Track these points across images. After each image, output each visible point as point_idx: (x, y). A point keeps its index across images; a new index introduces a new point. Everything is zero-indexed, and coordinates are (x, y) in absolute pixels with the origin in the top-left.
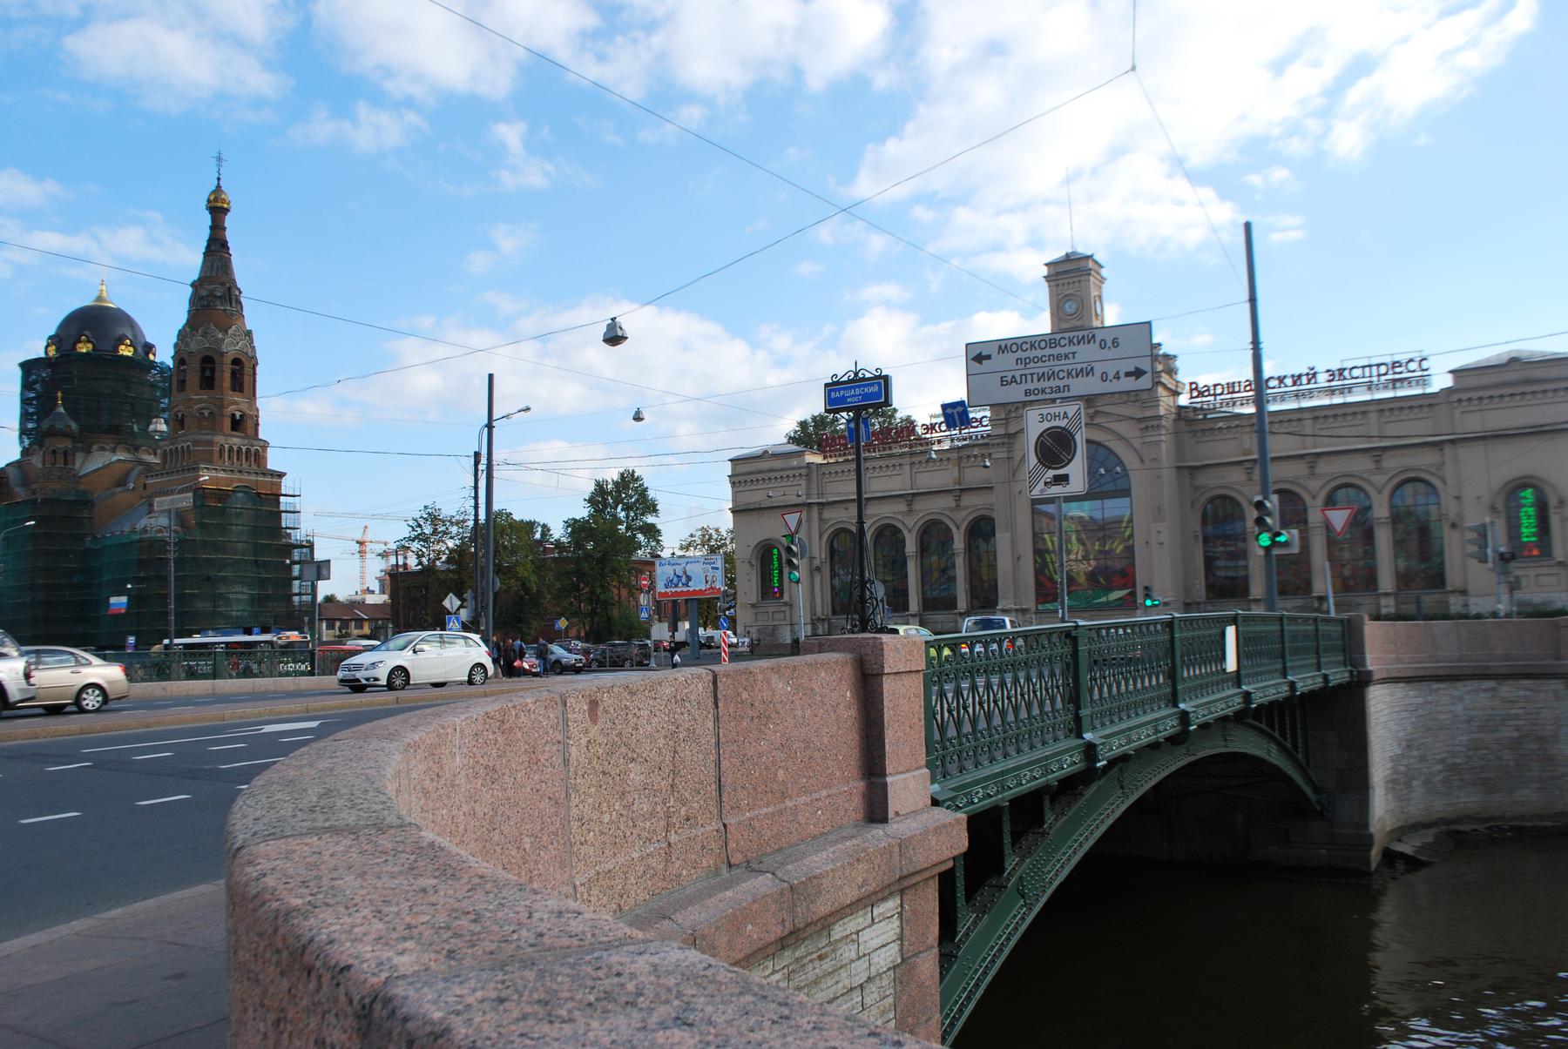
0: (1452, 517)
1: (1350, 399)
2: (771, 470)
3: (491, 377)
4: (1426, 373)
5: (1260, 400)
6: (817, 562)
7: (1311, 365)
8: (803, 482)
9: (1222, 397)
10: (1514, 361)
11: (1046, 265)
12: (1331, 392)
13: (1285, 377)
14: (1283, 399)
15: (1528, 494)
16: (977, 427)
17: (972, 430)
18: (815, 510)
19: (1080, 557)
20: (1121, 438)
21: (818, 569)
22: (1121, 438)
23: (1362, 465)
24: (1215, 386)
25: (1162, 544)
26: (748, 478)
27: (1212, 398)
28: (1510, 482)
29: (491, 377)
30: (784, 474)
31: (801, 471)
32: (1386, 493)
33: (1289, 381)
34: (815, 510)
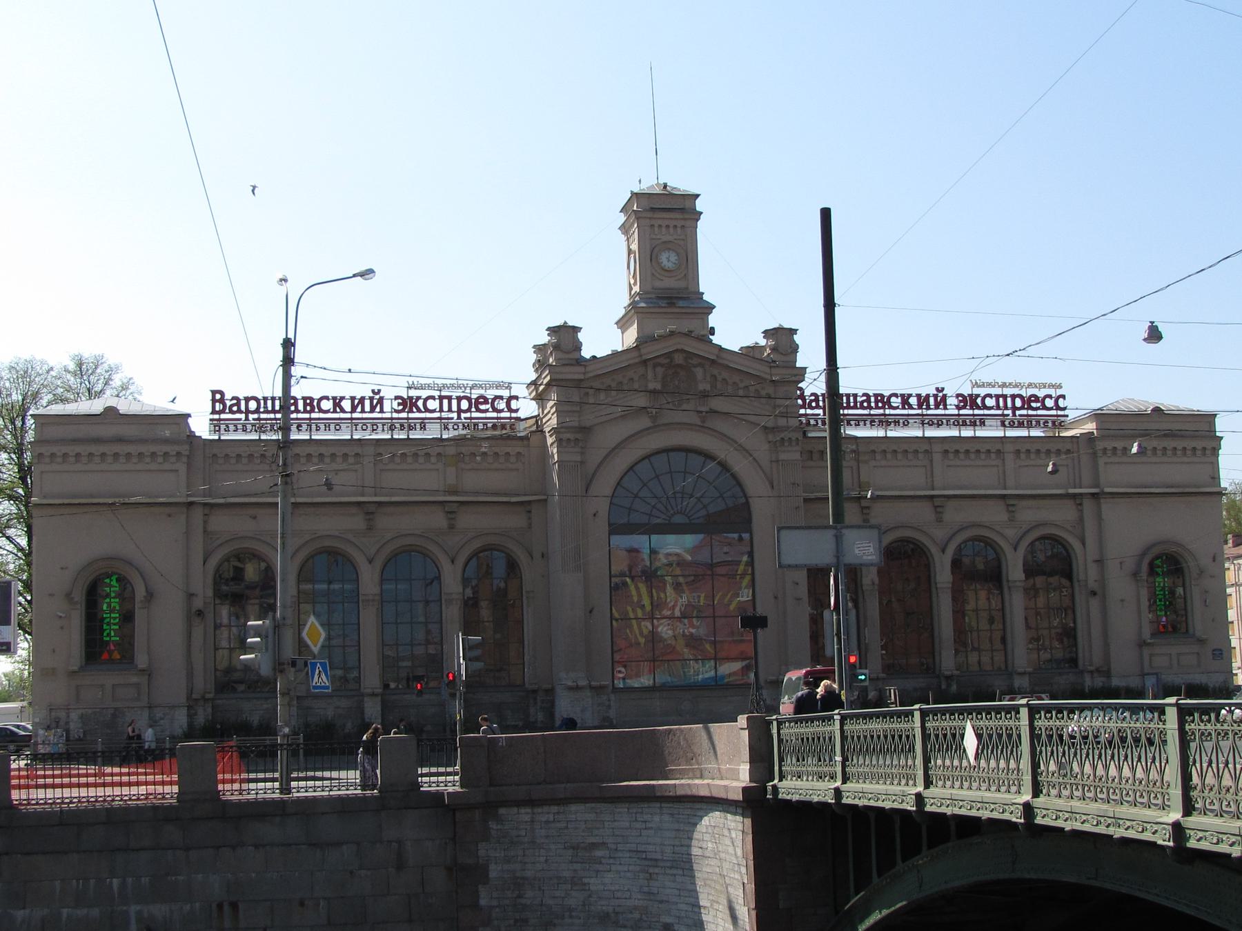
0: (1092, 584)
1: (981, 433)
2: (120, 440)
3: (826, 214)
4: (514, 415)
5: (836, 422)
6: (198, 603)
7: (940, 386)
8: (182, 468)
9: (468, 415)
10: (1157, 410)
11: (621, 212)
12: (960, 422)
13: (342, 398)
14: (906, 424)
15: (113, 586)
16: (486, 411)
17: (1031, 412)
18: (198, 514)
19: (677, 613)
20: (742, 449)
21: (200, 613)
22: (742, 449)
23: (994, 515)
24: (247, 399)
25: (799, 599)
26: (72, 450)
27: (243, 416)
28: (90, 564)
29: (826, 214)
30: (147, 449)
31: (177, 448)
32: (378, 563)
33: (346, 405)
34: (198, 514)
